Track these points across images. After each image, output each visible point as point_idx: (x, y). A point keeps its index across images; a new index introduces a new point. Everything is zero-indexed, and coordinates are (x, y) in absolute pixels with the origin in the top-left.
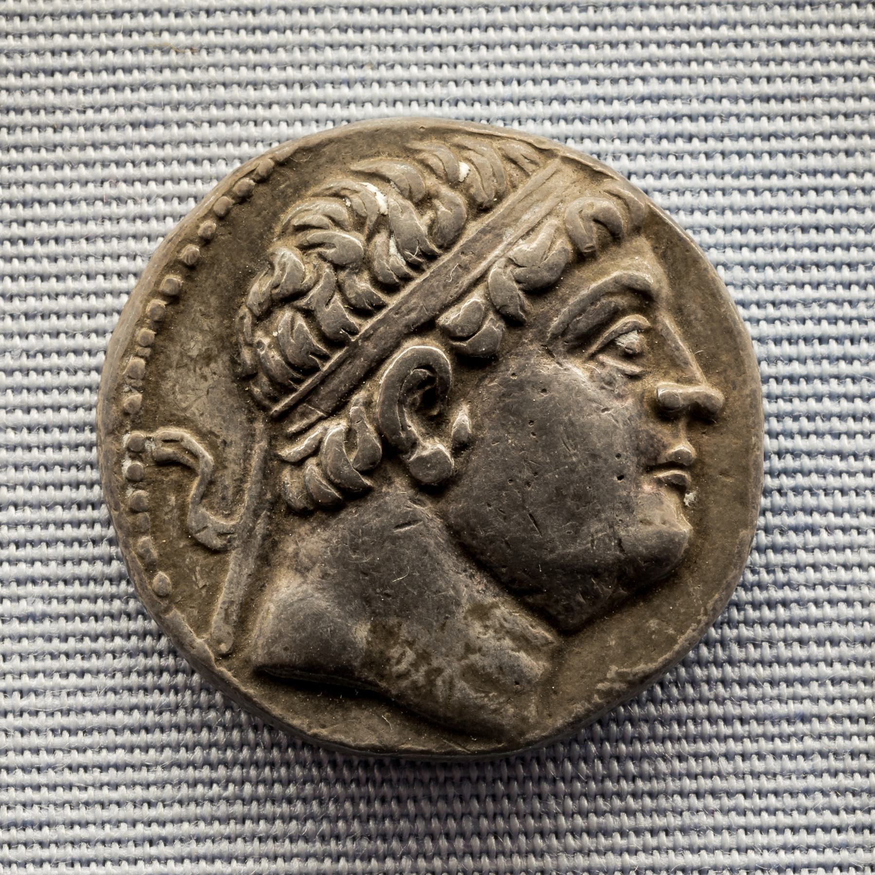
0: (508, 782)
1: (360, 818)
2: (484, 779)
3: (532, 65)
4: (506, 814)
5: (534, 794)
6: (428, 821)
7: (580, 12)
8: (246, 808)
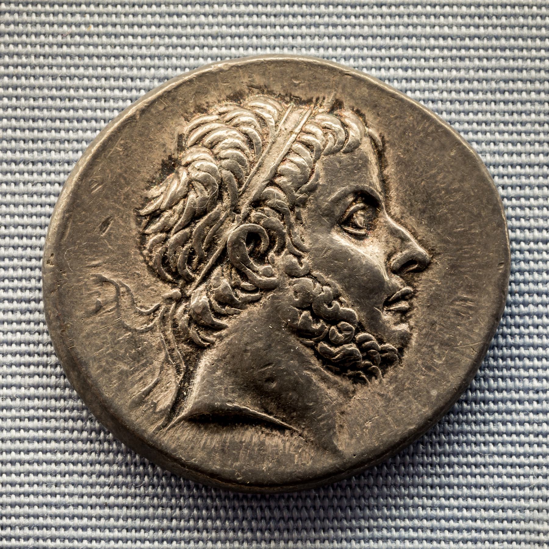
0: (322, 500)
1: (194, 518)
2: (328, 497)
3: (105, 90)
4: (295, 518)
5: (356, 506)
6: (287, 522)
7: (31, 69)
8: (146, 511)
